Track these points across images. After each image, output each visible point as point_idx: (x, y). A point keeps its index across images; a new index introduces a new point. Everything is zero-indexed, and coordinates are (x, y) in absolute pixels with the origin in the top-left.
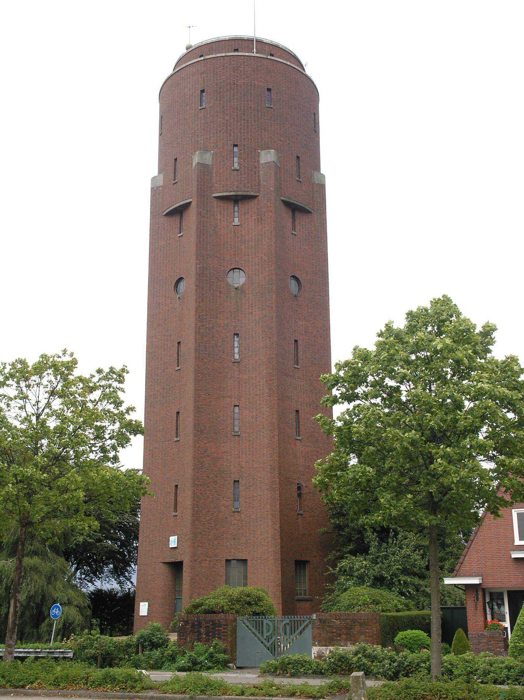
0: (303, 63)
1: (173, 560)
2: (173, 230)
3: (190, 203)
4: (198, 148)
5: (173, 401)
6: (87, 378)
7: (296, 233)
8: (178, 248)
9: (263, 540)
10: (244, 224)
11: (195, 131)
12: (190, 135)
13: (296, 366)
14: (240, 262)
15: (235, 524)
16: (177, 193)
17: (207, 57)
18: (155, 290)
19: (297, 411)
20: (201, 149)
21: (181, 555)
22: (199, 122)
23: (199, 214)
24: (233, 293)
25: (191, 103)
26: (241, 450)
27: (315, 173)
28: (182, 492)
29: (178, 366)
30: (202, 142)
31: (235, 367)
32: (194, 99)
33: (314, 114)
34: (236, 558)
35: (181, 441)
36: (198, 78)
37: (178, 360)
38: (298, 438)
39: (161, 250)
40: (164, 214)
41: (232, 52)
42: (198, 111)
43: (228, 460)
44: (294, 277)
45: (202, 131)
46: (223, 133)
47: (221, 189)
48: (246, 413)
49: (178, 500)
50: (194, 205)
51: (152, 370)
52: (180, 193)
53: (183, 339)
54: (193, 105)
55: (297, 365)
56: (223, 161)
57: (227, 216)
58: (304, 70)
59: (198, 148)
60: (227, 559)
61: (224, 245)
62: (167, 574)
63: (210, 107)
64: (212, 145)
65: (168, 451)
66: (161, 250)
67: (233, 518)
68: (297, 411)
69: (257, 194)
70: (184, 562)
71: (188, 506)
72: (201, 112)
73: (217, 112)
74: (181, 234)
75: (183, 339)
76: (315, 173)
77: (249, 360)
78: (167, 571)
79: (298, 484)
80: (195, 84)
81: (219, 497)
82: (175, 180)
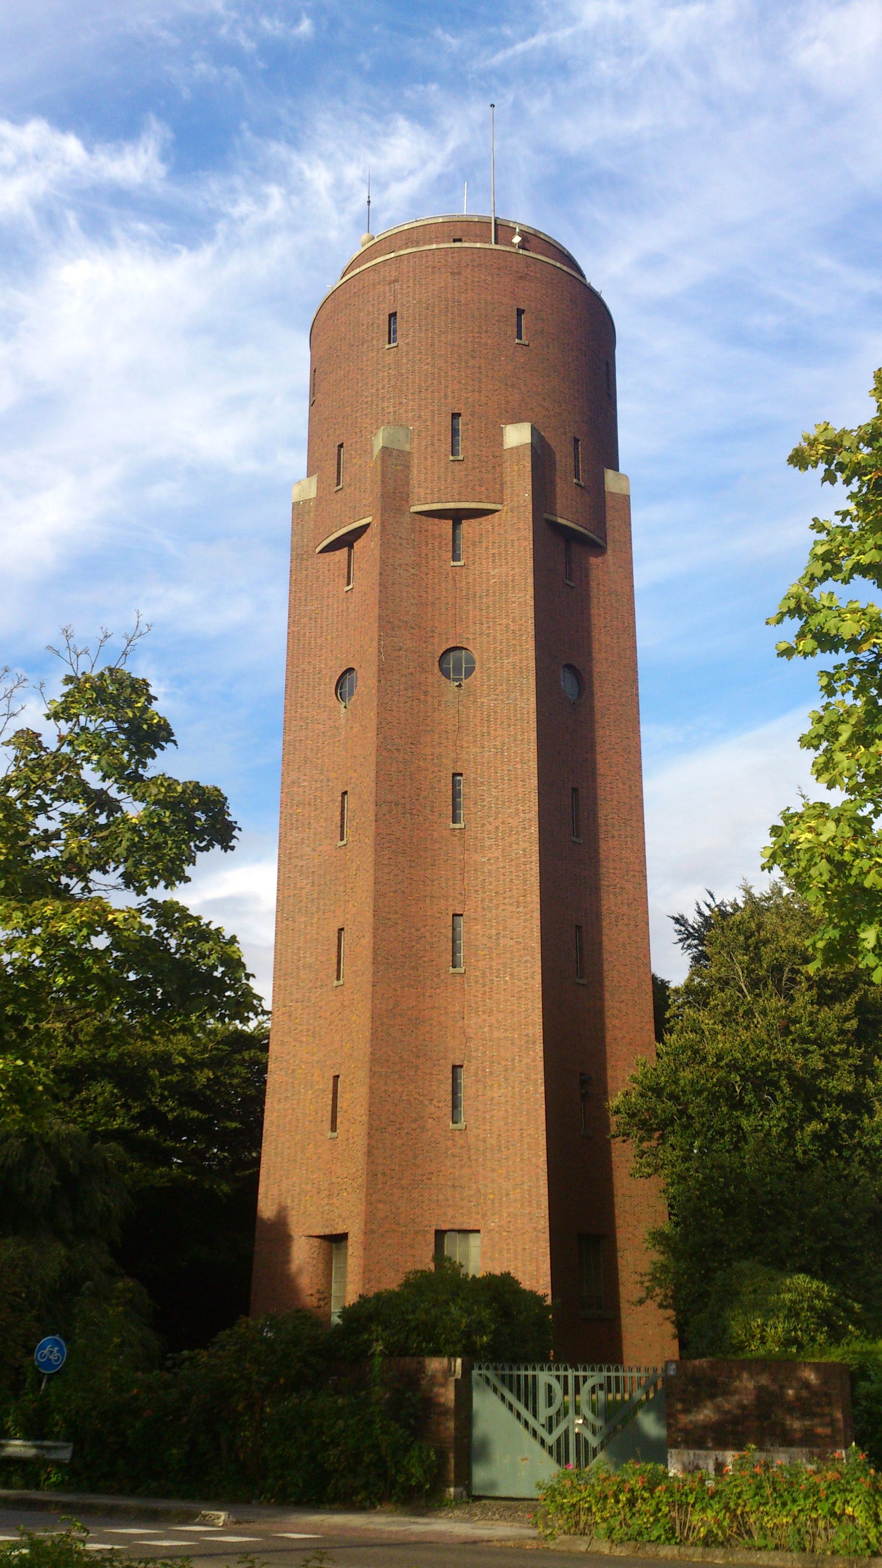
0: (585, 272)
1: (327, 1231)
2: (334, 581)
3: (367, 525)
4: (383, 421)
5: (332, 908)
6: (672, 986)
7: (573, 584)
8: (345, 613)
9: (430, 270)
10: (474, 564)
11: (377, 390)
12: (369, 399)
13: (574, 839)
14: (465, 636)
15: (454, 1156)
16: (344, 508)
17: (402, 252)
18: (299, 694)
19: (579, 928)
20: (388, 423)
21: (344, 1220)
22: (386, 374)
23: (385, 545)
24: (451, 696)
25: (370, 338)
26: (466, 1004)
27: (609, 474)
28: (348, 1089)
29: (342, 839)
30: (391, 409)
31: (454, 838)
32: (375, 330)
33: (607, 364)
34: (456, 1228)
35: (347, 985)
36: (384, 293)
37: (342, 826)
38: (581, 981)
39: (311, 619)
40: (318, 550)
41: (449, 242)
42: (383, 353)
43: (440, 1023)
44: (570, 667)
45: (391, 389)
46: (433, 392)
47: (429, 496)
48: (477, 930)
49: (339, 1105)
50: (375, 529)
51: (291, 849)
52: (347, 509)
53: (352, 786)
54: (375, 342)
55: (578, 836)
56: (432, 444)
57: (440, 548)
58: (583, 276)
59: (383, 421)
60: (439, 1228)
61: (433, 604)
62: (315, 1262)
63: (407, 344)
64: (410, 415)
65: (321, 1008)
66: (311, 619)
67: (450, 1143)
68: (579, 928)
69: (499, 507)
70: (350, 1236)
71: (360, 1119)
72: (389, 355)
73: (420, 353)
74: (350, 587)
75: (352, 786)
76: (609, 474)
77: (483, 825)
78: (315, 1255)
79: (581, 1074)
80: (379, 303)
81: (421, 1098)
82: (338, 484)
